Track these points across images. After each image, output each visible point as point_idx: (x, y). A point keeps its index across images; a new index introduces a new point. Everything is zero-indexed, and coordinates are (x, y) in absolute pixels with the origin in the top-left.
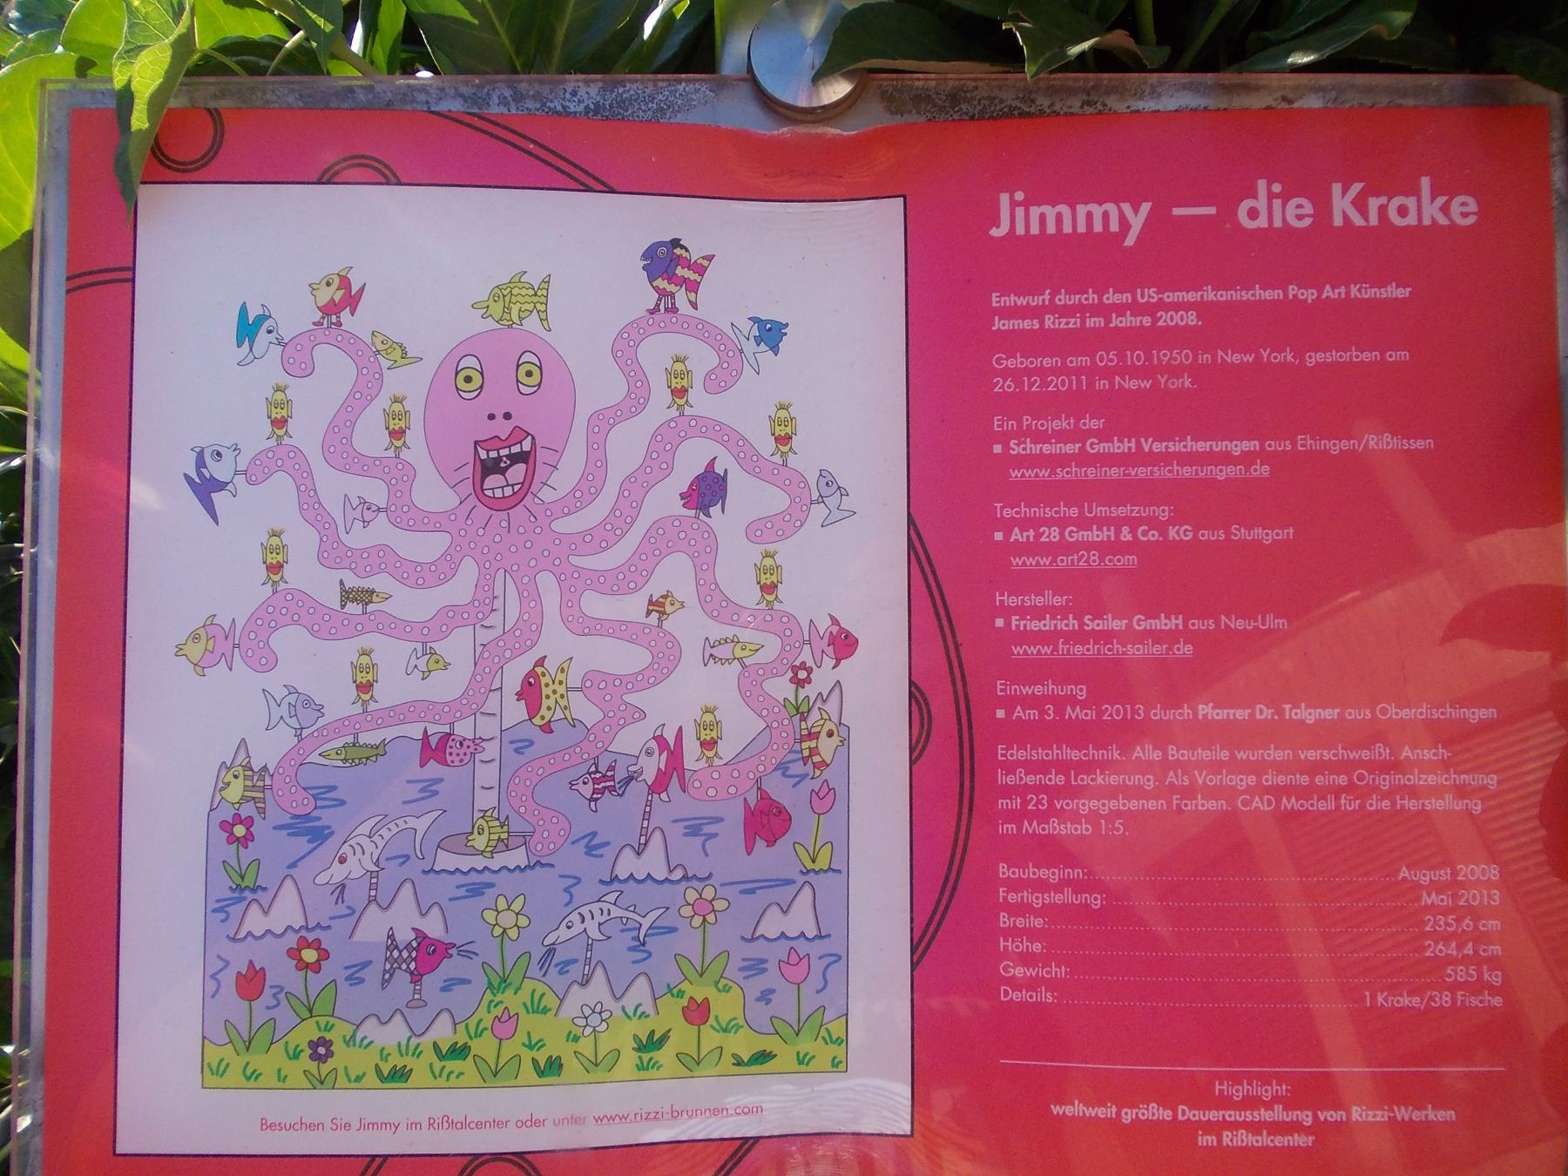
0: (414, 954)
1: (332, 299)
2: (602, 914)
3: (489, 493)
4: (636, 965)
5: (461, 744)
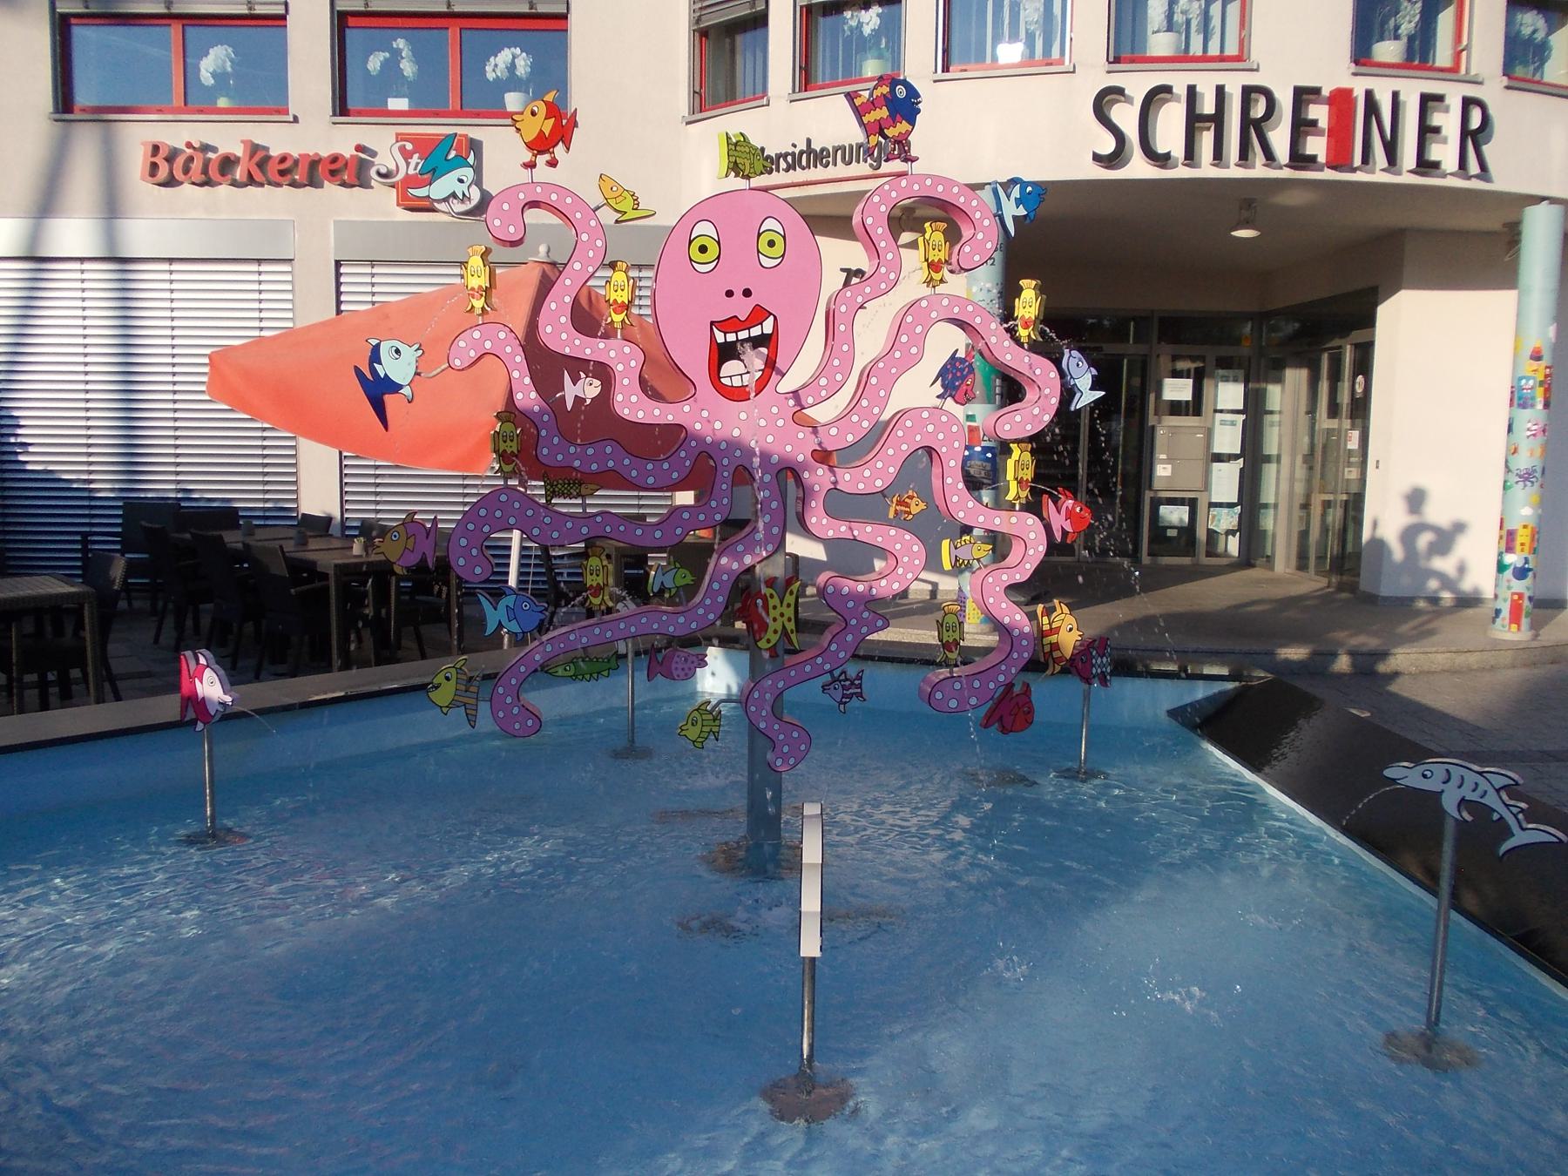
2: (1474, 791)
3: (726, 381)
5: (686, 660)
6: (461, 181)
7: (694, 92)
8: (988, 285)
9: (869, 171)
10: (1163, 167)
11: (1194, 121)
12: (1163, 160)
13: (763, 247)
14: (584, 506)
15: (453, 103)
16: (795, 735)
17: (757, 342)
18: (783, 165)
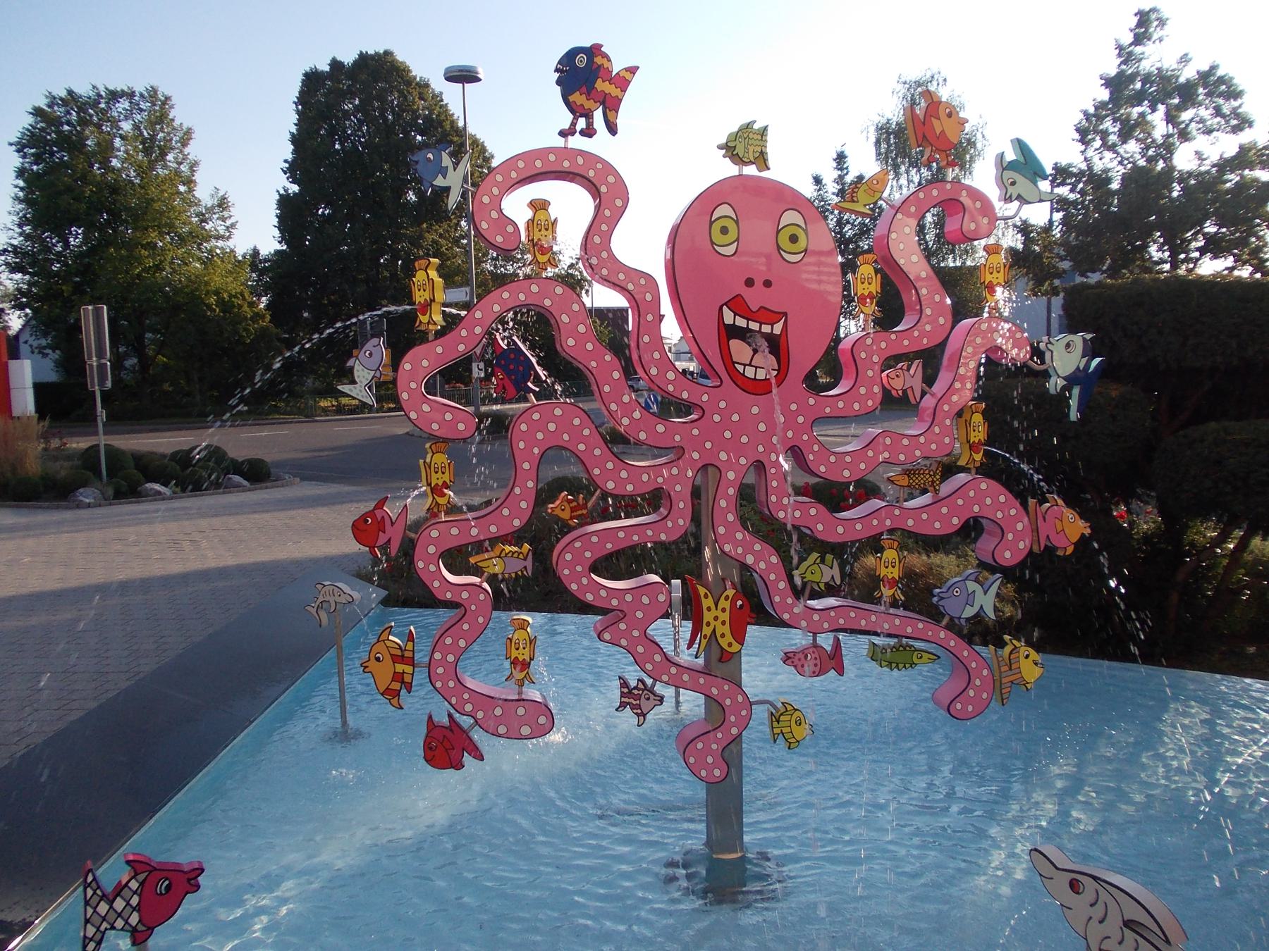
0: (135, 901)
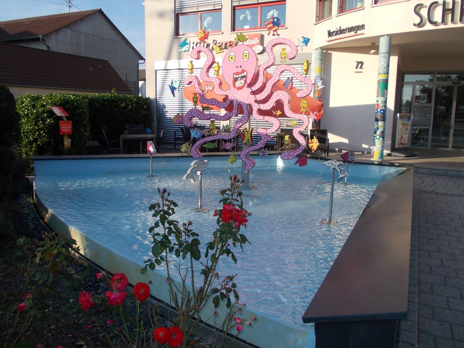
1: (202, 36)
4: (362, 71)
6: (187, 47)
7: (317, 16)
8: (384, 64)
9: (354, 34)
10: (436, 25)
11: (445, 11)
12: (435, 23)
13: (244, 56)
14: (210, 112)
15: (259, 26)
16: (250, 162)
17: (243, 77)
18: (334, 34)
